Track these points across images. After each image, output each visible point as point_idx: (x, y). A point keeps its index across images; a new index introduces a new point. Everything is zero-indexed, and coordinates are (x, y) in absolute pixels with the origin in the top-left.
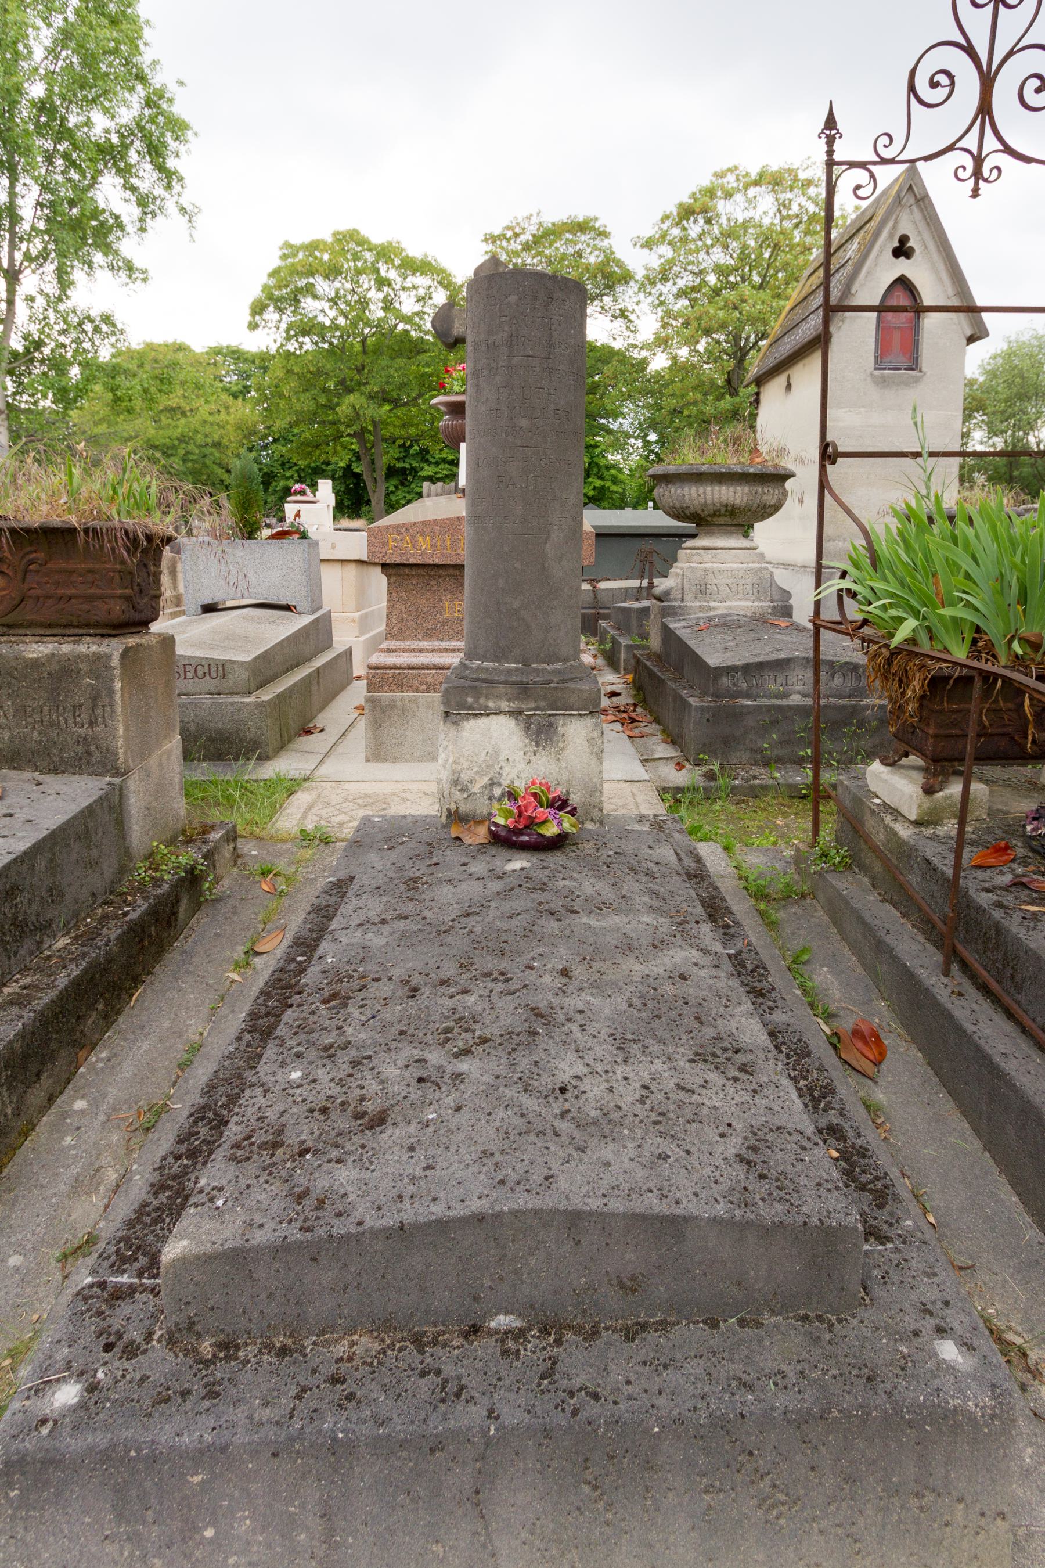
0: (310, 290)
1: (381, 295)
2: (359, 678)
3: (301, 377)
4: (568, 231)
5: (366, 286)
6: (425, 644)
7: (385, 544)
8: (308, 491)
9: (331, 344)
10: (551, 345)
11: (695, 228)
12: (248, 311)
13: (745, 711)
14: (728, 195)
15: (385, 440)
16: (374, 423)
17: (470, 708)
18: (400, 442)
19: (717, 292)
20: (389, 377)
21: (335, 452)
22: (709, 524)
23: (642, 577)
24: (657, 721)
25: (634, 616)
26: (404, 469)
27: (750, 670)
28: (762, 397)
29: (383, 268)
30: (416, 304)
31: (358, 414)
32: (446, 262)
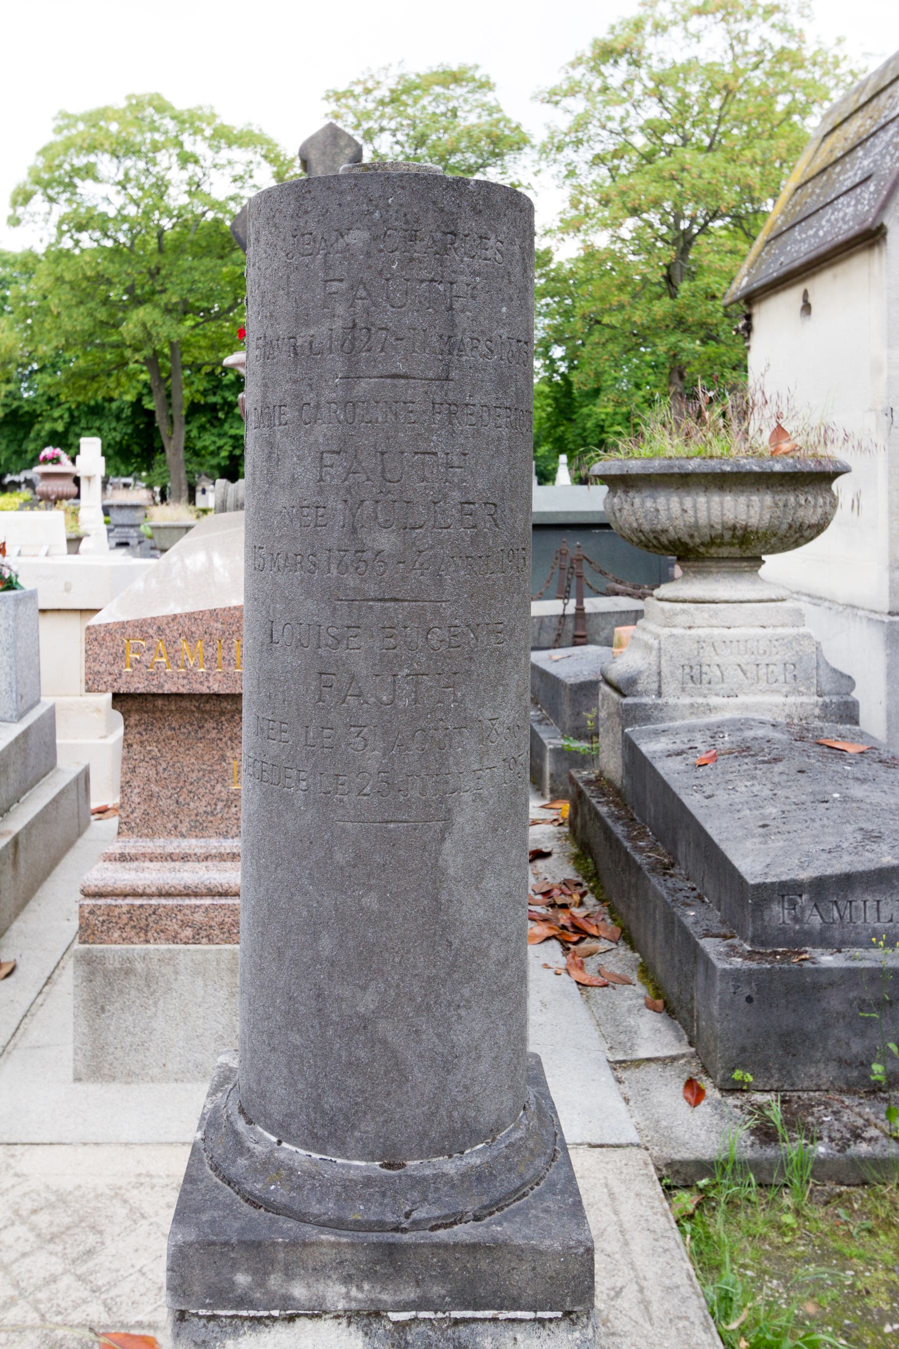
0: (89, 172)
1: (185, 175)
2: (102, 811)
3: (73, 286)
4: (437, 84)
5: (165, 164)
6: (192, 845)
7: (119, 656)
8: (64, 457)
9: (116, 240)
10: (451, 345)
11: (617, 74)
12: (7, 201)
13: (823, 979)
14: (660, 28)
15: (189, 367)
16: (172, 345)
17: (242, 1302)
18: (207, 369)
19: (649, 157)
20: (194, 282)
21: (119, 384)
22: (700, 558)
23: (564, 595)
24: (628, 938)
25: (565, 696)
26: (215, 404)
27: (825, 889)
28: (756, 321)
29: (185, 138)
30: (232, 183)
31: (149, 334)
32: (272, 132)
